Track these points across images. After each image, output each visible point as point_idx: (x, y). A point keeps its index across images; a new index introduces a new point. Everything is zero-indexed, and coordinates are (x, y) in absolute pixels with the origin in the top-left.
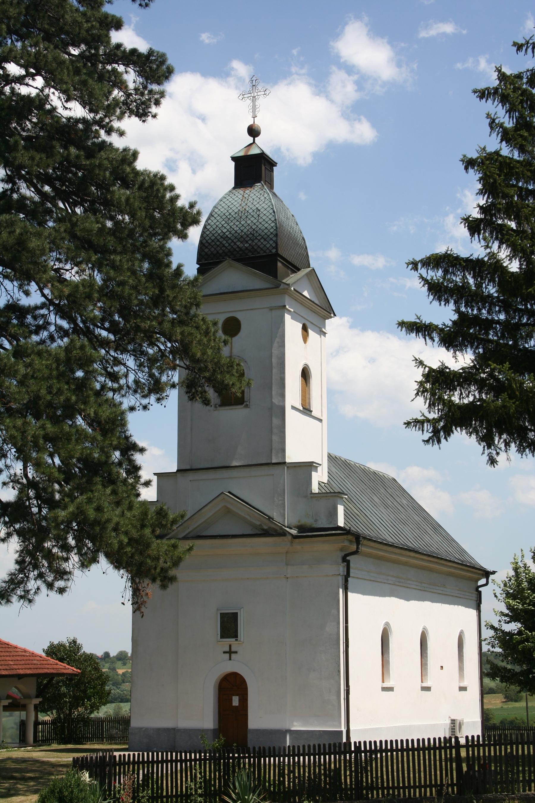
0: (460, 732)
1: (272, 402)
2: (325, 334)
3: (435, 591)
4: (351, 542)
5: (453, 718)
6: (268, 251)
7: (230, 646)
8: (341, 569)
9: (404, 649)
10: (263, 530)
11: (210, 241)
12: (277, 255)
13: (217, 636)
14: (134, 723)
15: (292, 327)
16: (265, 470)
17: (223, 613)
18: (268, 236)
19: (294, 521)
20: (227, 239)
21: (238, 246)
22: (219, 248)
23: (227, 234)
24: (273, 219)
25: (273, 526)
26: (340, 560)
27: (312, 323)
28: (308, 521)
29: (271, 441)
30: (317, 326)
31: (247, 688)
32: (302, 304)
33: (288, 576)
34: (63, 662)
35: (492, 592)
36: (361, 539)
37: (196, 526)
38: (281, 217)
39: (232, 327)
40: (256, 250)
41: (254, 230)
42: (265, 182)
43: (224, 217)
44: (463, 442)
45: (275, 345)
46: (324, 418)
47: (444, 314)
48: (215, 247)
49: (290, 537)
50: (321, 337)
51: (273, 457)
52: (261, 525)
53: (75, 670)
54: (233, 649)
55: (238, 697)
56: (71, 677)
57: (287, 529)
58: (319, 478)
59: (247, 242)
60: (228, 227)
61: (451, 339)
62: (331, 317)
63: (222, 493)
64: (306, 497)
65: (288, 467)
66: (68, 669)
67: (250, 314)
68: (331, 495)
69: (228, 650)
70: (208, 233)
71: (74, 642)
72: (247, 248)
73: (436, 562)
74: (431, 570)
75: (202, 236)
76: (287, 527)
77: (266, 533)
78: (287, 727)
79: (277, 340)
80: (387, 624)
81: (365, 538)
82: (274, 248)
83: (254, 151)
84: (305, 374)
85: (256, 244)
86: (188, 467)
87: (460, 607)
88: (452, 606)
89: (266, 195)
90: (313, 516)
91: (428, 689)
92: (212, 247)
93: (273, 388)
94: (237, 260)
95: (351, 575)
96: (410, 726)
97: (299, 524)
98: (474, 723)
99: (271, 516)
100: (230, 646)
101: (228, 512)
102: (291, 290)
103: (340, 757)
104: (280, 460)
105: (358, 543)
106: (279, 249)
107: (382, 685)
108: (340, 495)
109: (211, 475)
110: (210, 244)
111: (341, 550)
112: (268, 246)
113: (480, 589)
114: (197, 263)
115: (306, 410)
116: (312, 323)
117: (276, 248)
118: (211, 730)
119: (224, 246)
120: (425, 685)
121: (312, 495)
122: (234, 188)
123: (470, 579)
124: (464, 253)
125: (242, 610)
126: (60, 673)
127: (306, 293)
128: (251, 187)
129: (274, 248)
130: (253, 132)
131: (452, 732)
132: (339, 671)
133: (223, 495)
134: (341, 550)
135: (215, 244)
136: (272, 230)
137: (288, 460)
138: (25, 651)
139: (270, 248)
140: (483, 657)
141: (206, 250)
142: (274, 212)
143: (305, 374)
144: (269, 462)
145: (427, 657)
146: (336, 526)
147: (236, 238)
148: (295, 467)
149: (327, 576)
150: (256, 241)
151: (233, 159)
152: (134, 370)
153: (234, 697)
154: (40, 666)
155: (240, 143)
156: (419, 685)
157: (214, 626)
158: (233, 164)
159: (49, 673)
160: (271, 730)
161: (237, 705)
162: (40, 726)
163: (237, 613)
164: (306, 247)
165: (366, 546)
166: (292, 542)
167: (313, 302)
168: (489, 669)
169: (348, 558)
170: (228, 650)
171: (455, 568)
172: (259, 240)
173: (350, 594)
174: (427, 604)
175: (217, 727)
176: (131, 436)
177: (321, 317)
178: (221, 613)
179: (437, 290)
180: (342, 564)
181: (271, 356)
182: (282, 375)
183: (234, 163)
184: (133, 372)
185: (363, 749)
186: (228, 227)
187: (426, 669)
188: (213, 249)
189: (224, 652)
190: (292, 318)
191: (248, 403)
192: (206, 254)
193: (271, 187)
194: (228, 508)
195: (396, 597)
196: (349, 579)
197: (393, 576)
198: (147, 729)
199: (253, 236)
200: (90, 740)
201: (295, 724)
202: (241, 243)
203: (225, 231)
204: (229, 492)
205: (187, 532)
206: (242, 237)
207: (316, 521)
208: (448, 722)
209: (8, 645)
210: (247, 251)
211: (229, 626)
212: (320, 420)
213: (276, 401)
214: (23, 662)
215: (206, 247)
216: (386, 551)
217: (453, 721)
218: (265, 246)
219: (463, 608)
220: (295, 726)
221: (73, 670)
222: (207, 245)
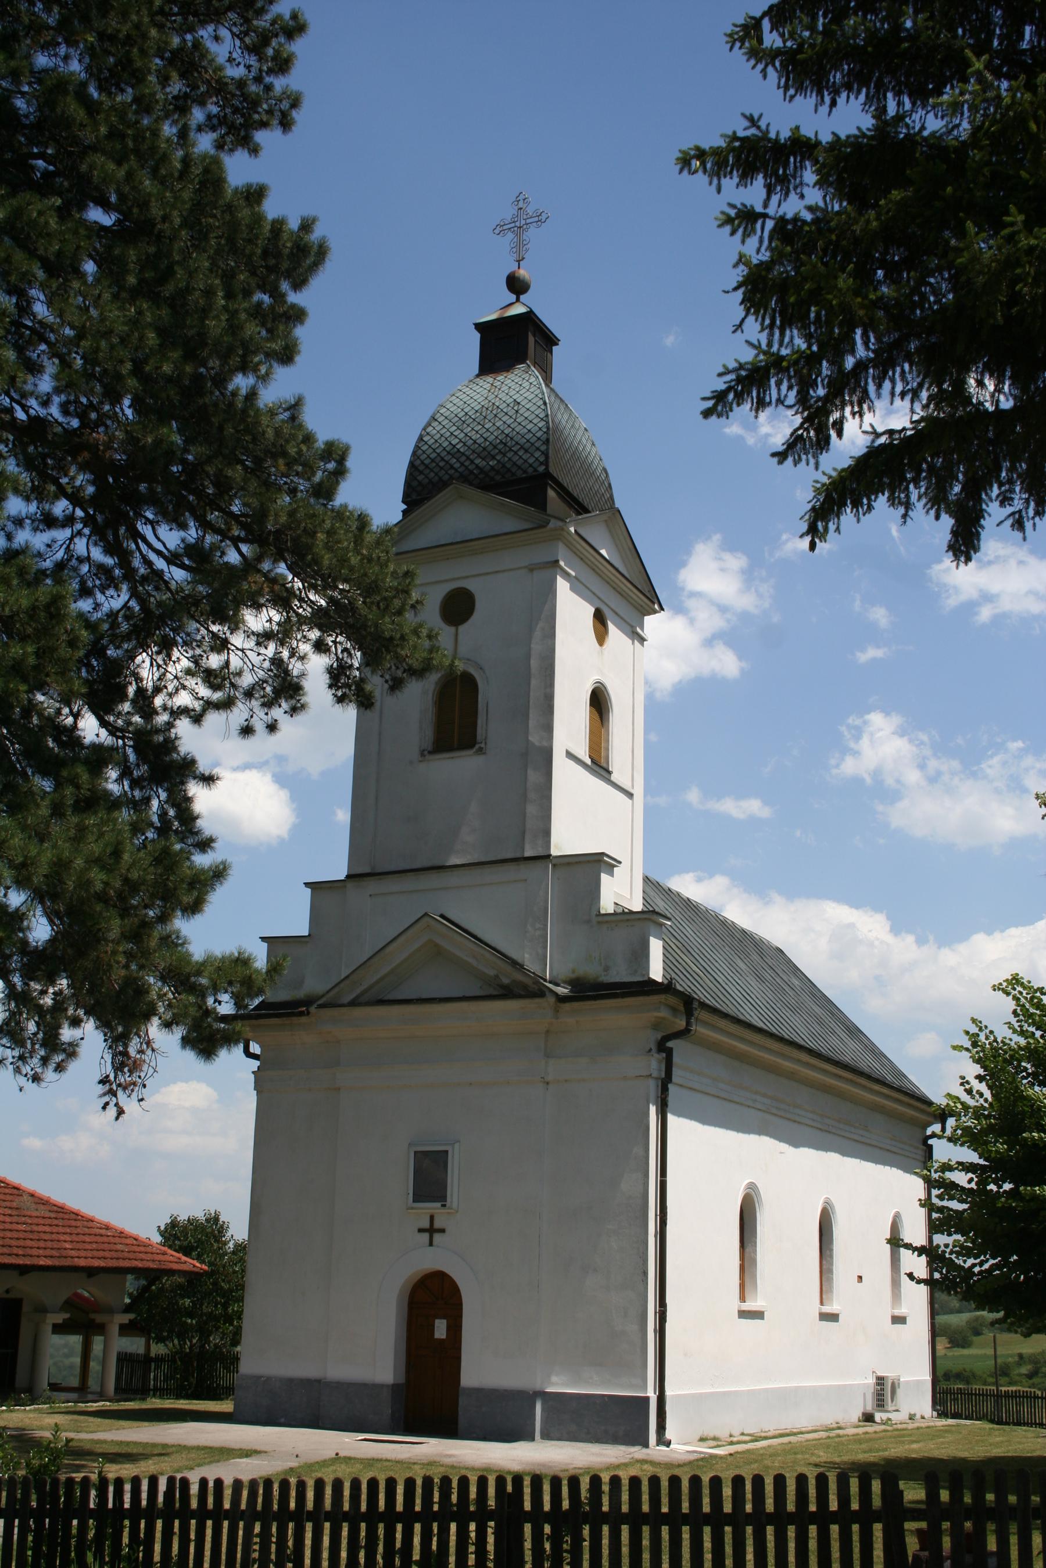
0: (892, 1401)
1: (528, 741)
2: (642, 640)
3: (847, 1135)
4: (674, 1010)
5: (879, 1374)
6: (530, 470)
7: (432, 1218)
8: (655, 1064)
10: (503, 987)
11: (427, 462)
12: (547, 475)
15: (572, 611)
16: (511, 872)
17: (426, 1154)
18: (532, 444)
19: (565, 971)
20: (459, 455)
21: (477, 466)
22: (443, 472)
23: (458, 447)
24: (542, 415)
25: (519, 977)
27: (616, 613)
28: (592, 971)
29: (524, 815)
30: (625, 621)
31: (461, 1304)
32: (594, 569)
33: (549, 1078)
36: (695, 1005)
37: (375, 979)
39: (458, 607)
40: (509, 470)
41: (507, 435)
42: (535, 364)
43: (456, 419)
45: (538, 634)
46: (638, 791)
48: (436, 470)
49: (552, 1000)
50: (633, 643)
51: (527, 847)
52: (497, 976)
53: (198, 1265)
54: (437, 1225)
55: (445, 1321)
56: (193, 1278)
57: (550, 986)
58: (620, 892)
59: (493, 458)
60: (462, 435)
62: (655, 612)
63: (426, 914)
64: (589, 921)
65: (554, 866)
66: (185, 1262)
67: (494, 589)
68: (637, 924)
70: (425, 448)
71: (216, 1219)
72: (492, 467)
73: (851, 1081)
74: (840, 1095)
75: (414, 453)
76: (550, 982)
77: (507, 992)
78: (538, 1387)
79: (541, 625)
80: (752, 1186)
81: (703, 1005)
82: (541, 463)
85: (510, 459)
86: (367, 870)
87: (894, 1169)
88: (880, 1167)
89: (532, 379)
91: (833, 1317)
92: (432, 470)
93: (531, 715)
95: (674, 1079)
96: (797, 1388)
97: (573, 976)
98: (918, 1383)
99: (520, 961)
100: (432, 1218)
101: (436, 953)
102: (569, 533)
103: (444, 1532)
104: (540, 852)
105: (689, 1013)
106: (551, 464)
107: (740, 1306)
108: (655, 917)
109: (409, 883)
110: (427, 467)
111: (656, 1026)
112: (531, 461)
113: (930, 1142)
114: (403, 502)
115: (599, 765)
116: (616, 613)
117: (546, 463)
118: (388, 1386)
119: (452, 467)
120: (826, 1309)
121: (600, 919)
122: (478, 376)
123: (912, 1122)
125: (457, 1146)
126: (164, 1270)
127: (603, 552)
128: (508, 371)
129: (541, 463)
131: (878, 1400)
132: (645, 1273)
133: (426, 919)
134: (656, 1026)
135: (437, 465)
136: (539, 434)
137: (554, 852)
138: (107, 1227)
139: (535, 465)
141: (420, 478)
142: (545, 403)
144: (518, 855)
145: (831, 1256)
146: (646, 978)
147: (474, 451)
148: (569, 864)
150: (510, 455)
151: (479, 327)
152: (242, 650)
154: (126, 1255)
156: (815, 1308)
157: (400, 1180)
158: (477, 336)
160: (506, 1391)
161: (444, 1337)
163: (447, 1152)
164: (610, 485)
165: (705, 1024)
166: (556, 1011)
167: (617, 570)
168: (946, 1283)
169: (670, 1044)
171: (887, 1097)
172: (516, 453)
173: (671, 1119)
174: (834, 1157)
175: (402, 1380)
176: (176, 738)
177: (635, 607)
178: (415, 1152)
180: (656, 1055)
181: (528, 657)
183: (478, 335)
184: (240, 653)
185: (527, 1506)
186: (462, 435)
187: (830, 1280)
188: (432, 475)
189: (421, 1230)
190: (571, 589)
191: (483, 745)
192: (420, 483)
194: (436, 945)
195: (771, 1136)
196: (670, 1086)
197: (765, 1095)
198: (269, 1379)
199: (505, 445)
201: (554, 1379)
202: (483, 459)
203: (454, 442)
204: (442, 916)
205: (358, 991)
206: (484, 449)
207: (607, 969)
208: (871, 1381)
209: (77, 1215)
210: (492, 474)
212: (630, 795)
213: (534, 738)
214: (94, 1246)
215: (421, 473)
216: (751, 1043)
217: (880, 1380)
218: (526, 461)
219: (900, 1172)
220: (554, 1384)
221: (194, 1266)
222: (421, 468)
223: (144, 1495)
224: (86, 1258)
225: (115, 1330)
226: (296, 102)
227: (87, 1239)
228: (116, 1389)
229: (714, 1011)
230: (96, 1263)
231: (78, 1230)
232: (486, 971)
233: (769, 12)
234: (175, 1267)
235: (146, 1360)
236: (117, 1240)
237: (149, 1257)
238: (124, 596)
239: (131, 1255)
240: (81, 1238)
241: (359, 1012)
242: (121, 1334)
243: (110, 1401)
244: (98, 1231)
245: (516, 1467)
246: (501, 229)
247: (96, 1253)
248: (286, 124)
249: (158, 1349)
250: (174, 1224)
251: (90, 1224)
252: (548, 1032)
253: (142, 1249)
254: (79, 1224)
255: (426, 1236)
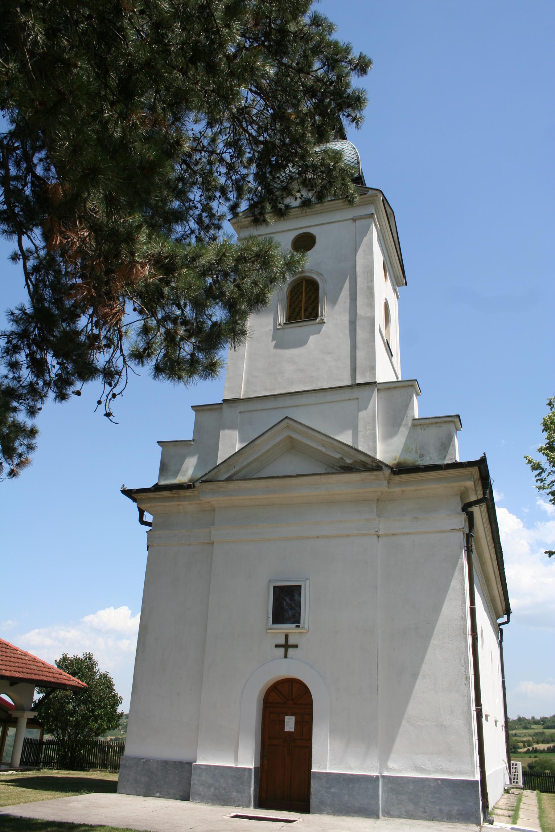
7: (287, 636)
13: (268, 620)
14: (129, 751)
25: (363, 458)
26: (460, 509)
28: (412, 458)
33: (381, 533)
34: (74, 677)
37: (245, 463)
52: (342, 458)
53: (81, 682)
54: (291, 642)
55: (293, 718)
56: (77, 690)
69: (282, 642)
71: (90, 658)
77: (347, 469)
90: (416, 450)
100: (287, 636)
101: (292, 446)
125: (308, 581)
133: (287, 421)
138: (26, 655)
140: (11, 755)
146: (453, 461)
148: (389, 388)
149: (442, 531)
153: (287, 718)
154: (37, 672)
159: (45, 681)
162: (44, 746)
163: (300, 586)
170: (282, 642)
175: (259, 765)
182: (370, 284)
189: (277, 646)
200: (92, 766)
207: (422, 456)
209: (7, 645)
221: (79, 683)
224: (10, 671)
225: (23, 722)
227: (12, 660)
228: (21, 761)
230: (17, 675)
231: (7, 654)
232: (332, 454)
234: (67, 682)
235: (41, 743)
236: (31, 663)
237: (51, 675)
239: (40, 673)
240: (8, 659)
241: (232, 485)
242: (27, 727)
243: (16, 770)
244: (19, 656)
247: (17, 669)
249: (47, 737)
251: (15, 652)
252: (378, 500)
253: (47, 670)
254: (8, 650)
255: (282, 650)
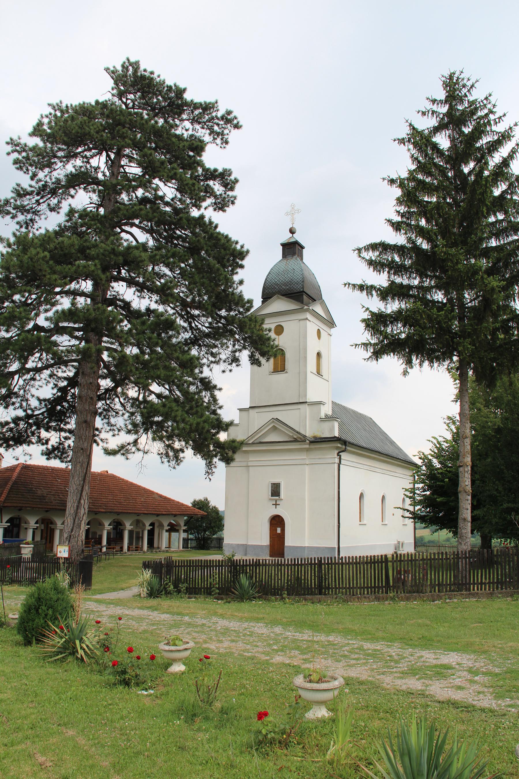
9: (372, 504)
35: (349, 291)
38: (306, 273)
39: (279, 330)
44: (392, 363)
47: (382, 280)
56: (203, 517)
61: (385, 294)
81: (350, 443)
83: (292, 240)
84: (319, 355)
94: (283, 295)
117: (303, 288)
124: (392, 242)
130: (292, 231)
143: (319, 355)
155: (286, 237)
179: (376, 265)
193: (302, 259)
205: (254, 439)
208: (396, 542)
211: (276, 490)
223: (433, 573)
226: (235, 198)
229: (353, 444)
233: (365, 247)
238: (190, 334)
245: (150, 560)
246: (287, 214)
248: (233, 203)
249: (191, 536)
250: (195, 501)
